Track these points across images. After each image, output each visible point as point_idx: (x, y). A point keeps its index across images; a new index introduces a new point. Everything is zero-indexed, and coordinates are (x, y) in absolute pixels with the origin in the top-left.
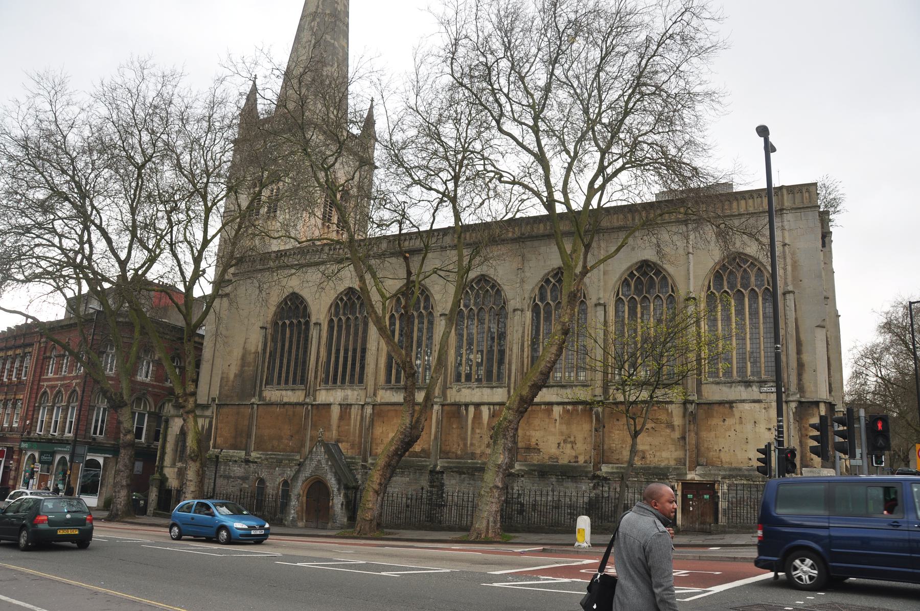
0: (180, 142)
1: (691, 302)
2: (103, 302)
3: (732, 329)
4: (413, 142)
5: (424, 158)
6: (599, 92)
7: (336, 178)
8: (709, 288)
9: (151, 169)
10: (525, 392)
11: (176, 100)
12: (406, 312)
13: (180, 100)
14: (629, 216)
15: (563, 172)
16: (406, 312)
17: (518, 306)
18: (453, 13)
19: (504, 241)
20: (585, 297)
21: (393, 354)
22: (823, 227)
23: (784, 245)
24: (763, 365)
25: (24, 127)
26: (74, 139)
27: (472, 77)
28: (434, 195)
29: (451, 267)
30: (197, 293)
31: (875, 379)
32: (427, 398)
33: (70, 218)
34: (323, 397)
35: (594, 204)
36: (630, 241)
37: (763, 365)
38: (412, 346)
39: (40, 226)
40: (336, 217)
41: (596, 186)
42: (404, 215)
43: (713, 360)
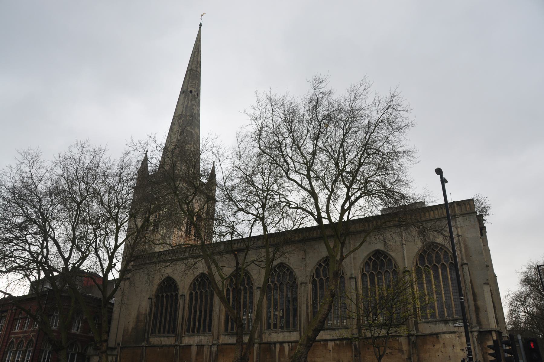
0: (103, 189)
1: (407, 274)
2: (53, 284)
3: (433, 289)
4: (238, 186)
5: (244, 196)
6: (344, 153)
7: (194, 208)
8: (417, 264)
9: (85, 204)
10: (310, 334)
11: (101, 165)
12: (236, 287)
13: (104, 165)
14: (366, 224)
15: (326, 200)
16: (236, 287)
17: (303, 281)
18: (259, 113)
19: (293, 242)
20: (343, 274)
21: (229, 313)
22: (480, 224)
23: (459, 236)
24: (454, 310)
25: (13, 181)
26: (41, 187)
27: (271, 148)
28: (251, 217)
29: (262, 259)
30: (110, 277)
31: (524, 314)
32: (251, 339)
33: (36, 233)
34: (186, 341)
35: (345, 218)
36: (368, 239)
37: (454, 310)
38: (240, 308)
39: (18, 238)
40: (194, 231)
41: (346, 208)
42: (234, 229)
43: (423, 308)
